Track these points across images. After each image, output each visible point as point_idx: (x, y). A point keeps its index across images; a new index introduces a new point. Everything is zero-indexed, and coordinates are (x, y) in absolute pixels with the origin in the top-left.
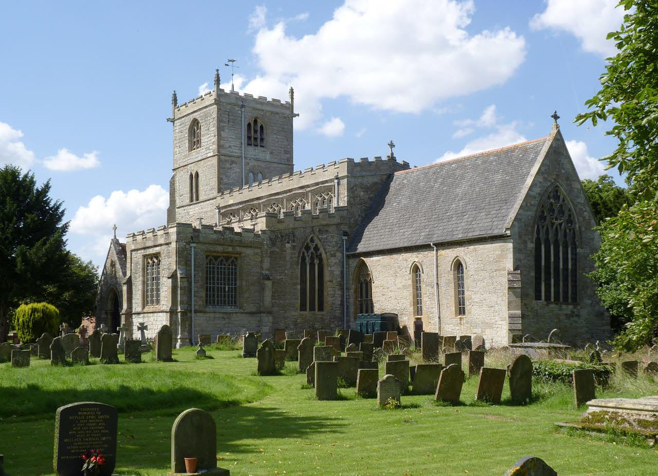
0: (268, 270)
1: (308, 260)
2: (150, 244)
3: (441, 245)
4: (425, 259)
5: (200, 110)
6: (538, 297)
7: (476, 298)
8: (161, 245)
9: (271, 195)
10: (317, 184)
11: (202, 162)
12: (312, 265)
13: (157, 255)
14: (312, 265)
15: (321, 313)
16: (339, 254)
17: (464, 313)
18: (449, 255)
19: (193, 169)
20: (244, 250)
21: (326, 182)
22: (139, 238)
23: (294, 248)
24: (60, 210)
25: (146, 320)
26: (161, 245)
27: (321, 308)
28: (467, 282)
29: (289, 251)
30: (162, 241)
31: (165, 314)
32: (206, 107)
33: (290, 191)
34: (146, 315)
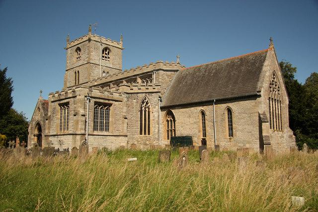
0: (125, 113)
1: (143, 108)
2: (63, 97)
3: (219, 102)
4: (232, 105)
5: (81, 43)
6: (141, 134)
7: (240, 128)
8: (70, 98)
9: (118, 80)
10: (143, 73)
11: (81, 67)
12: (145, 111)
13: (67, 104)
14: (145, 111)
15: (149, 136)
16: (157, 107)
17: (232, 136)
18: (200, 108)
19: (77, 69)
20: (111, 102)
21: (149, 72)
22: (56, 95)
23: (137, 102)
24: (12, 81)
25: (62, 139)
26: (70, 98)
27: (149, 134)
28: (234, 120)
29: (135, 104)
30: (70, 95)
31: (71, 136)
32: (84, 42)
33: (129, 77)
34: (59, 136)
